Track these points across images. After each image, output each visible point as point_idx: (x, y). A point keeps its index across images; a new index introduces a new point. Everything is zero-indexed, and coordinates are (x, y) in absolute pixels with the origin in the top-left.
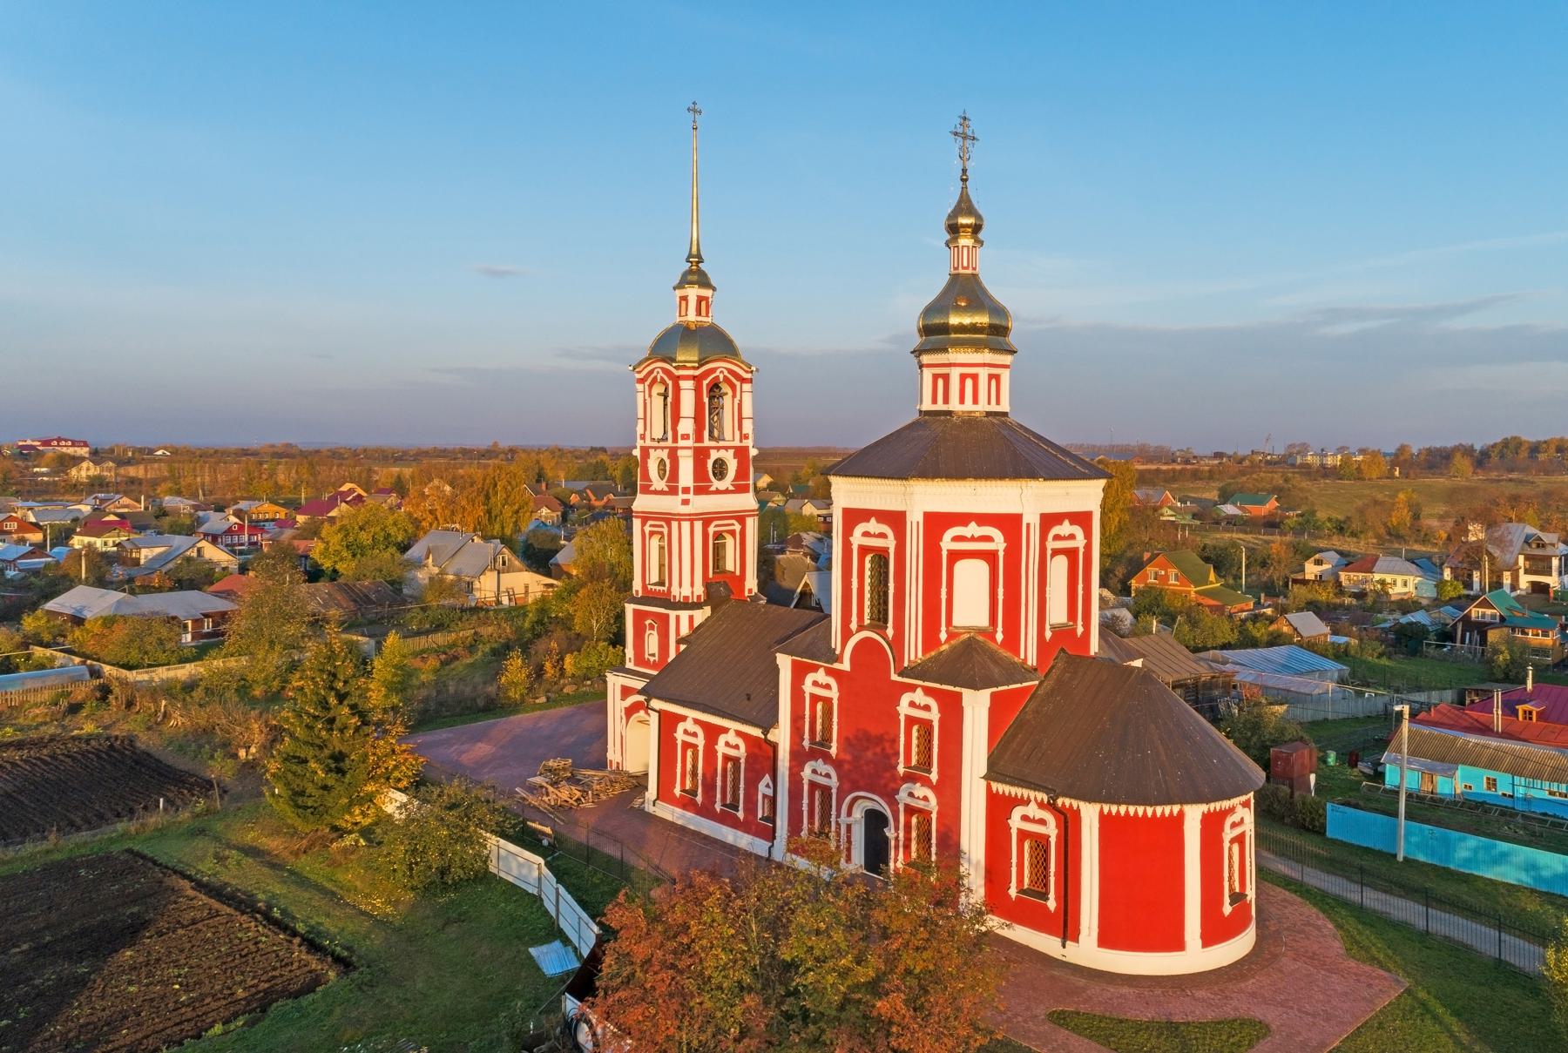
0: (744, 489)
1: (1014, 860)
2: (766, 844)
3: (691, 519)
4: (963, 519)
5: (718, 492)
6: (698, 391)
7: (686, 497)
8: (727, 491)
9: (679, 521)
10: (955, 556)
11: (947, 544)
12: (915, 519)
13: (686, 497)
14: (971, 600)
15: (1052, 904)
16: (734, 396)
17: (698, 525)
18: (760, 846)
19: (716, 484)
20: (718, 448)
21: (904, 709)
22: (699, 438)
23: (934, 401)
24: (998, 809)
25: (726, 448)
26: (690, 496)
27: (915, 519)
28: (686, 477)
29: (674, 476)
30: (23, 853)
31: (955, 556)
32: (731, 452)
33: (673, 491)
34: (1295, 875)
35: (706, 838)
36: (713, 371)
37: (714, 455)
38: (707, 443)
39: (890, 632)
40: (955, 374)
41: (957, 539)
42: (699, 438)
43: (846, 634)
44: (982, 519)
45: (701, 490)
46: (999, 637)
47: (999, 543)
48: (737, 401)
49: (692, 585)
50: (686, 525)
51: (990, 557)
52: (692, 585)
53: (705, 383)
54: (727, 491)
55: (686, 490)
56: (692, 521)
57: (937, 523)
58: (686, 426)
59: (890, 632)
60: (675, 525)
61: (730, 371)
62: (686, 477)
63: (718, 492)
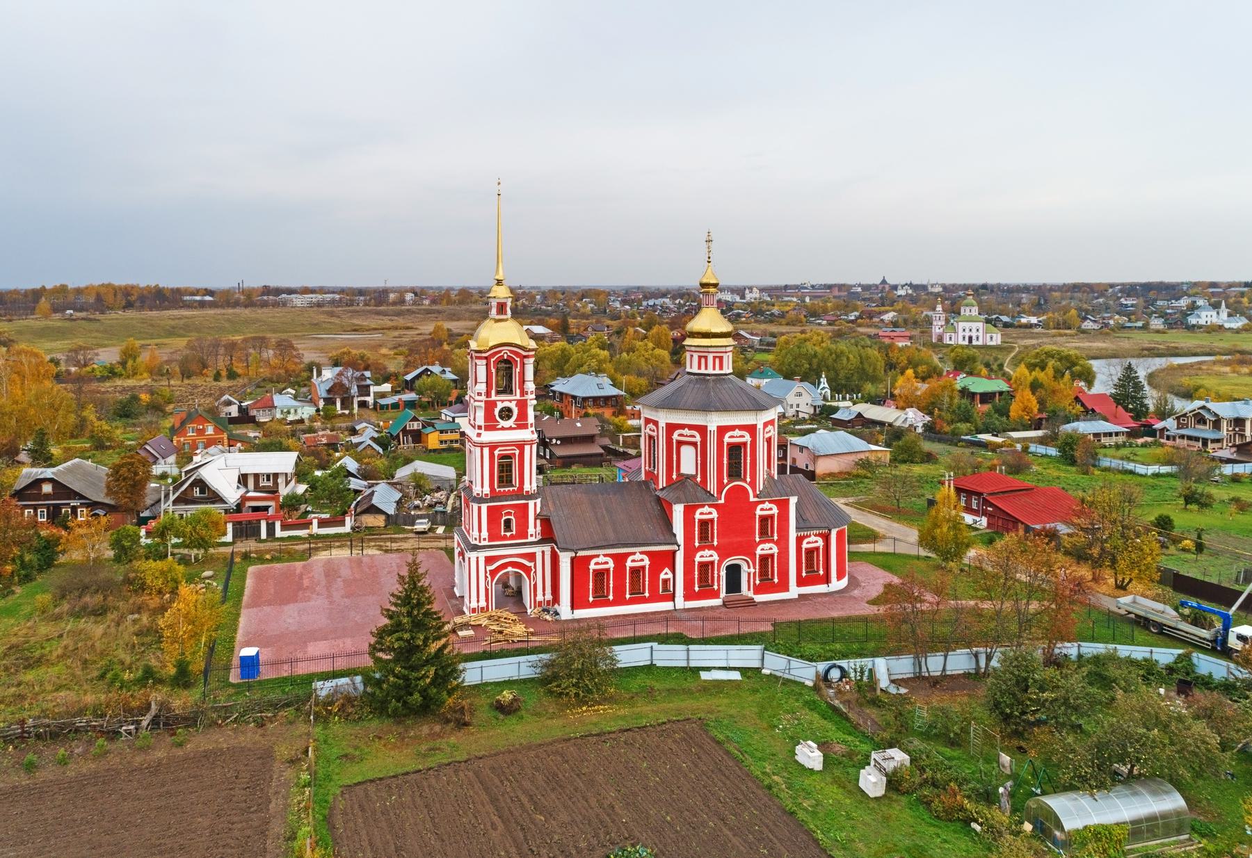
0: (525, 427)
2: (671, 603)
3: (482, 445)
4: (682, 427)
5: (503, 429)
10: (680, 443)
11: (675, 436)
12: (662, 424)
14: (688, 462)
15: (821, 572)
17: (486, 451)
18: (667, 606)
19: (503, 423)
22: (488, 394)
23: (699, 368)
24: (799, 540)
26: (482, 431)
27: (662, 424)
31: (680, 443)
35: (624, 615)
38: (494, 397)
39: (748, 480)
40: (710, 357)
41: (680, 435)
42: (488, 394)
43: (721, 486)
45: (488, 428)
47: (698, 439)
51: (694, 444)
54: (511, 428)
55: (480, 428)
56: (482, 448)
57: (671, 428)
63: (503, 429)
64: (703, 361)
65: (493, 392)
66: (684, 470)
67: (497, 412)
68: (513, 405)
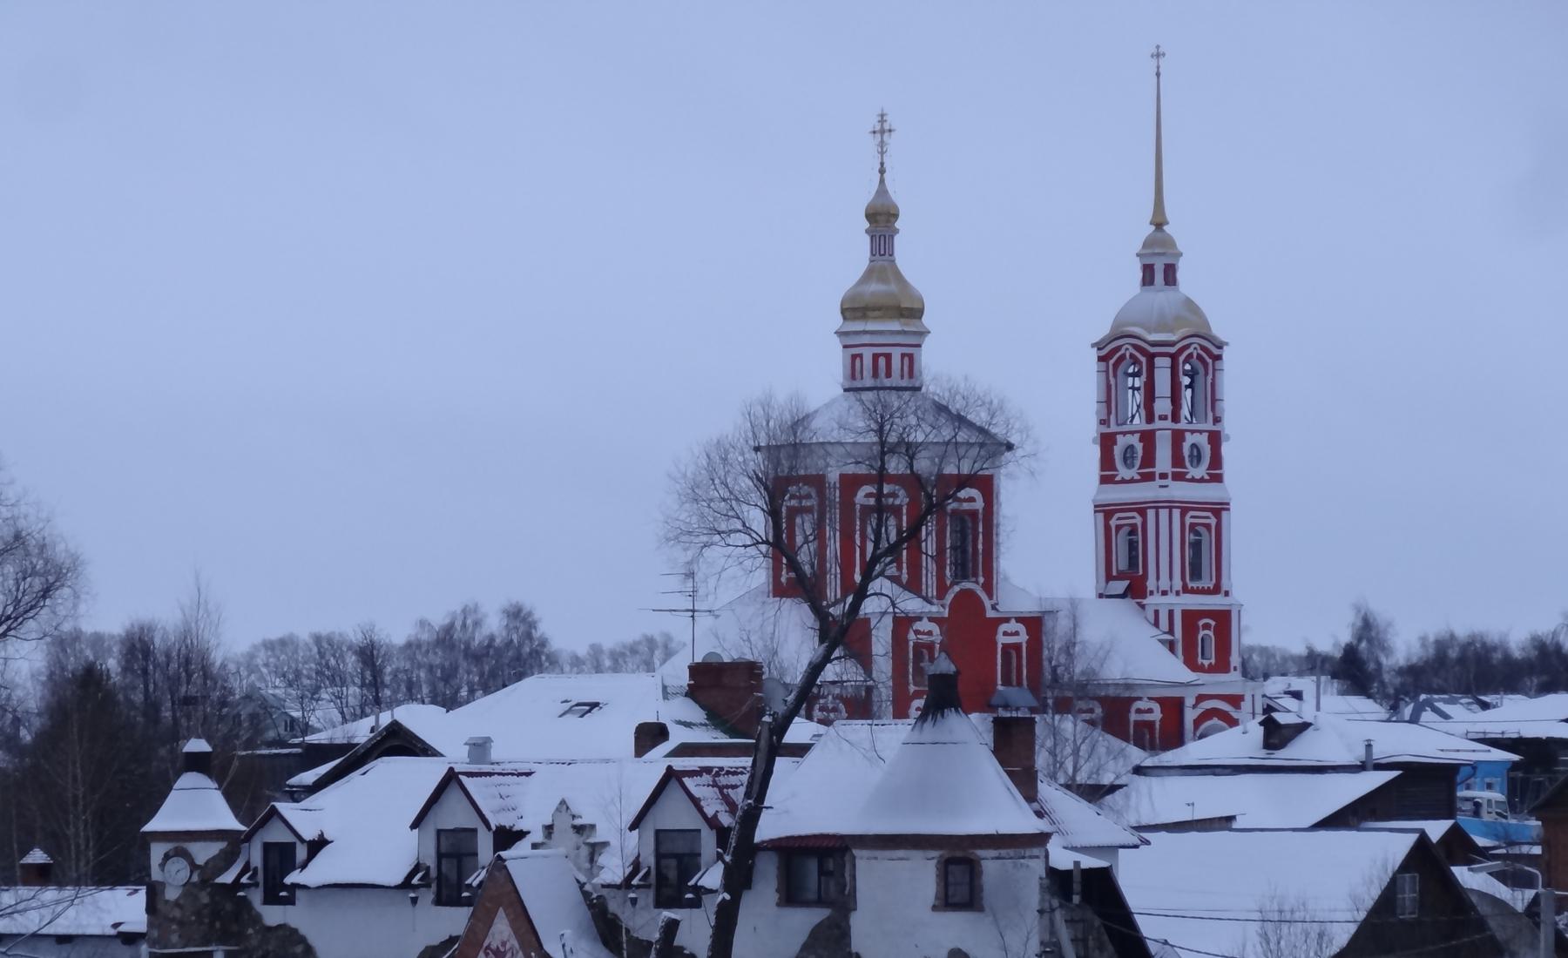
5: (1123, 481)
7: (1163, 482)
8: (1132, 481)
9: (1157, 508)
16: (1206, 374)
17: (1176, 513)
20: (1124, 433)
21: (1001, 640)
22: (1176, 417)
26: (1168, 482)
28: (1163, 460)
29: (1149, 459)
30: (369, 722)
32: (1137, 436)
33: (1148, 478)
34: (1518, 866)
37: (1190, 439)
45: (1179, 477)
49: (1158, 578)
50: (1164, 514)
52: (1158, 578)
54: (1202, 480)
55: (1163, 476)
56: (1170, 508)
58: (1163, 406)
59: (981, 580)
60: (1151, 514)
61: (1135, 347)
62: (1163, 460)
63: (1123, 481)
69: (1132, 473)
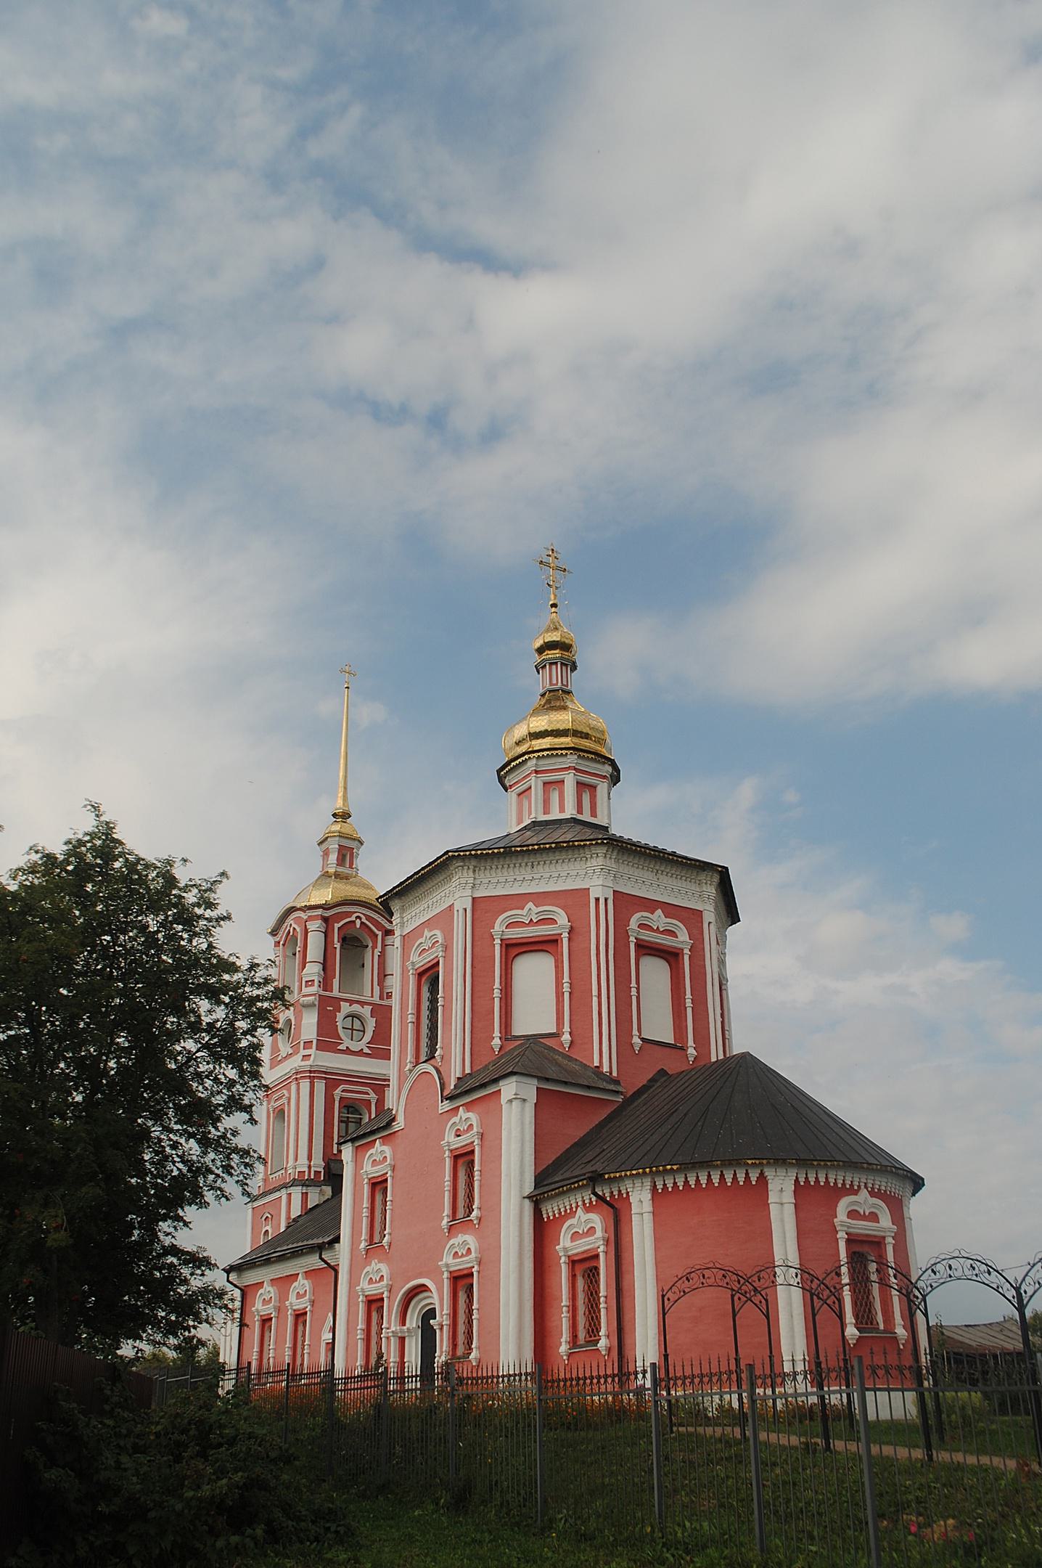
1: (565, 1301)
5: (348, 1051)
6: (327, 934)
7: (307, 1052)
8: (360, 1053)
10: (514, 949)
13: (307, 1052)
17: (320, 1086)
20: (351, 1002)
25: (362, 1004)
31: (514, 949)
36: (349, 914)
38: (335, 993)
42: (326, 984)
44: (540, 898)
45: (322, 1046)
46: (566, 1037)
48: (377, 953)
49: (310, 1159)
53: (337, 926)
54: (360, 1053)
55: (308, 1044)
61: (368, 918)
63: (348, 1051)
64: (555, 796)
65: (336, 982)
66: (520, 1029)
67: (340, 1016)
68: (366, 1011)
69: (361, 1045)
